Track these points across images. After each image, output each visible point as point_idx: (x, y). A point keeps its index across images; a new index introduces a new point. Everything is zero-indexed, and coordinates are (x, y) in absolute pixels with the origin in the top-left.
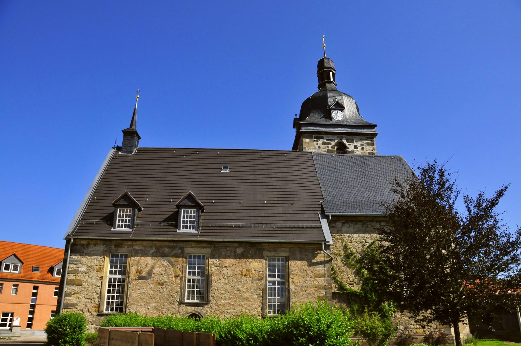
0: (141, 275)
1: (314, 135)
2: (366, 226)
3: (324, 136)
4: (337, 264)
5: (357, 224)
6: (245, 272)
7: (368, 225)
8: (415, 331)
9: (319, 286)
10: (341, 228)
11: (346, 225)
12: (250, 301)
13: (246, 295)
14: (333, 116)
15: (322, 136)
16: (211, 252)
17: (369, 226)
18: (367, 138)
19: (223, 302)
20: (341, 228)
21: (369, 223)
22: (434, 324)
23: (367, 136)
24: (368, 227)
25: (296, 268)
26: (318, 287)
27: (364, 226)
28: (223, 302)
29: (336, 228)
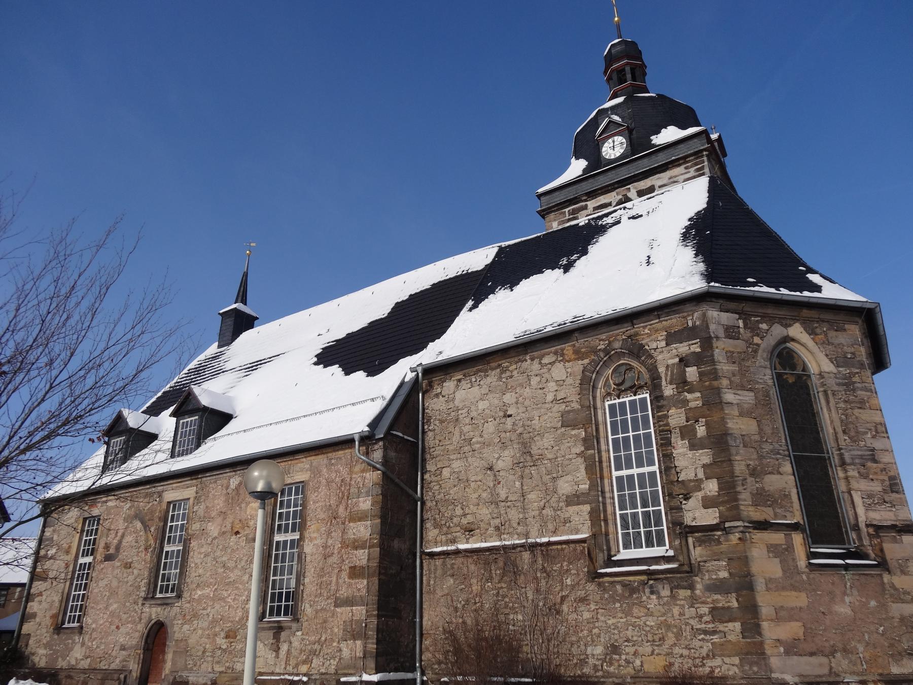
0: (109, 552)
1: (567, 210)
2: (508, 374)
3: (588, 203)
4: (441, 483)
5: (488, 376)
6: (237, 527)
7: (512, 372)
8: (638, 662)
9: (355, 541)
10: (454, 393)
11: (465, 384)
12: (237, 588)
13: (232, 576)
14: (604, 154)
15: (583, 204)
16: (197, 493)
17: (515, 373)
18: (686, 168)
19: (199, 593)
20: (454, 393)
21: (514, 367)
22: (703, 640)
23: (684, 163)
24: (511, 377)
25: (317, 505)
26: (357, 545)
27: (503, 376)
28: (199, 593)
29: (443, 396)
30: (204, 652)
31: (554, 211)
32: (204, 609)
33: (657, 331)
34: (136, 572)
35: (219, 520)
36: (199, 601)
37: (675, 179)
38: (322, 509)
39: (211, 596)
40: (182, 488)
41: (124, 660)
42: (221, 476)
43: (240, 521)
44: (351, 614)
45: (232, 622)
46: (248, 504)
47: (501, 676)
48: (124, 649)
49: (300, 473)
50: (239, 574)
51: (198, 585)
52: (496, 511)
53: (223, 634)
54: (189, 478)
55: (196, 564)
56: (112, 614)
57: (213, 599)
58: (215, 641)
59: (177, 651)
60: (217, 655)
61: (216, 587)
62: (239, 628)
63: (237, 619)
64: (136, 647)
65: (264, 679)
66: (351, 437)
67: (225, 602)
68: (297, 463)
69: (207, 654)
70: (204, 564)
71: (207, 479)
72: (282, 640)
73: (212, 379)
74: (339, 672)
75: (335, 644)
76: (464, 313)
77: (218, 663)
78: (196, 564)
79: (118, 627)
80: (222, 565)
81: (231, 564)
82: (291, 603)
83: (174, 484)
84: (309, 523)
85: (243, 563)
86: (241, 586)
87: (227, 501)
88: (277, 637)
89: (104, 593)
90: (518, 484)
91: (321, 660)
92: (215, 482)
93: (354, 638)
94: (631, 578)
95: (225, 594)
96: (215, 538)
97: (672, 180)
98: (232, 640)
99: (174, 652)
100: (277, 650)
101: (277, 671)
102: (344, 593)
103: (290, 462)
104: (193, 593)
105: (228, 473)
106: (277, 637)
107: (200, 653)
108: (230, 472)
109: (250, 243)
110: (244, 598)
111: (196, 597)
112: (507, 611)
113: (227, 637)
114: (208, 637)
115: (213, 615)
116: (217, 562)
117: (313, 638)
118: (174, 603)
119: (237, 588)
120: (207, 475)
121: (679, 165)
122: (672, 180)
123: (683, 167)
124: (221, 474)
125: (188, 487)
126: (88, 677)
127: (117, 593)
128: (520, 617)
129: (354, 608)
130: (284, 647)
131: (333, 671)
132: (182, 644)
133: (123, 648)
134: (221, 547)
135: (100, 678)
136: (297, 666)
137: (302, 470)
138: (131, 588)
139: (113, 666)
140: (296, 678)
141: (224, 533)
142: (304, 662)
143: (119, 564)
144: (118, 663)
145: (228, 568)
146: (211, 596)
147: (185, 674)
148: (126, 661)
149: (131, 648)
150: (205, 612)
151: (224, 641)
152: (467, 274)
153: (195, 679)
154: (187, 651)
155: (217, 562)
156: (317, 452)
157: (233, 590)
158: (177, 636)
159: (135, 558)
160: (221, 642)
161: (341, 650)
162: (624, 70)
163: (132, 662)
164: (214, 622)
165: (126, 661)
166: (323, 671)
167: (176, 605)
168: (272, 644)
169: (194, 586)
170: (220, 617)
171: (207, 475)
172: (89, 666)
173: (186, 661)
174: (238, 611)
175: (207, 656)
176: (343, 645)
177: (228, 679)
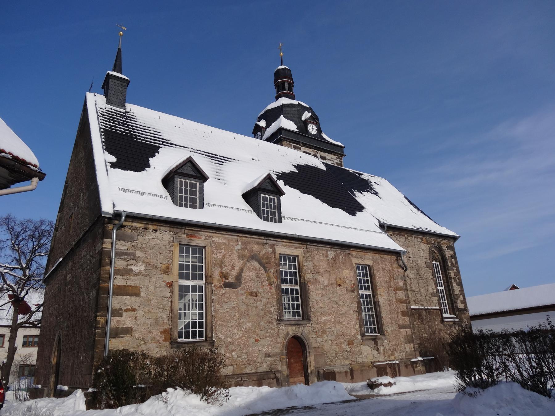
6: (339, 282)
12: (348, 317)
23: (337, 155)
30: (336, 354)
31: (287, 141)
32: (329, 328)
33: (445, 244)
34: (264, 300)
35: (327, 275)
36: (325, 323)
37: (333, 160)
38: (383, 282)
39: (333, 320)
40: (291, 247)
41: (272, 364)
42: (321, 248)
43: (340, 278)
44: (406, 332)
45: (350, 336)
46: (342, 270)
47: (144, 384)
48: (269, 356)
49: (368, 260)
50: (347, 309)
51: (322, 314)
52: (413, 294)
53: (346, 343)
54: (300, 243)
55: (316, 300)
56: (248, 330)
57: (334, 323)
58: (341, 347)
59: (317, 355)
60: (345, 355)
61: (334, 315)
62: (355, 339)
63: (353, 334)
64: (281, 354)
65: (379, 365)
66: (400, 251)
67: (343, 324)
68: (366, 255)
69: (339, 355)
70: (322, 301)
71: (311, 247)
72: (379, 345)
73: (169, 146)
74: (407, 358)
75: (403, 346)
76: (357, 199)
77: (347, 359)
78: (316, 300)
79: (257, 341)
80: (336, 303)
81: (341, 303)
82: (365, 327)
83: (285, 242)
84: (378, 288)
85: (348, 304)
86: (350, 316)
87: (328, 264)
88: (376, 343)
89: (233, 314)
90: (418, 285)
91: (399, 353)
92: (318, 250)
93: (410, 343)
94: (450, 323)
95: (342, 320)
96: (326, 286)
97: (332, 159)
98: (352, 346)
99: (314, 355)
100: (378, 350)
101: (381, 360)
102: (401, 322)
103: (362, 253)
104: (319, 318)
105: (327, 248)
106: (376, 343)
107: (334, 355)
108: (329, 248)
109: (122, 26)
110: (353, 323)
111: (322, 321)
112: (422, 333)
113: (349, 344)
114: (337, 344)
115: (337, 332)
116: (331, 300)
117: (393, 343)
118: (306, 324)
119: (348, 317)
120: (314, 245)
121: (335, 155)
122: (332, 159)
123: (335, 156)
124: (322, 247)
125: (296, 248)
126: (241, 380)
127: (248, 314)
128: (426, 335)
129: (407, 329)
130: (382, 348)
131: (405, 358)
132: (319, 350)
133: (267, 355)
134: (331, 292)
135: (255, 379)
136: (389, 357)
137: (369, 259)
138: (263, 312)
139: (261, 369)
140: (394, 362)
141: (331, 284)
142: (392, 355)
143: (243, 292)
144: (266, 367)
145: (340, 305)
146: (333, 320)
147: (327, 367)
148: (274, 364)
149: (276, 355)
150: (330, 330)
151: (348, 346)
152: (316, 168)
153: (338, 369)
154: (325, 354)
155: (331, 300)
156: (377, 252)
157: (346, 318)
158: (314, 345)
159: (261, 290)
160: (345, 347)
161: (405, 348)
162: (284, 83)
163: (280, 365)
164: (338, 336)
165: (274, 364)
166: (401, 358)
167: (308, 325)
168: (375, 347)
169: (319, 314)
170: (341, 333)
171: (314, 245)
172: (233, 372)
173: (325, 360)
174: (352, 330)
175: (339, 356)
176: (406, 346)
177: (359, 367)
